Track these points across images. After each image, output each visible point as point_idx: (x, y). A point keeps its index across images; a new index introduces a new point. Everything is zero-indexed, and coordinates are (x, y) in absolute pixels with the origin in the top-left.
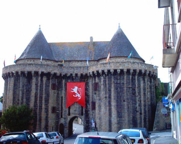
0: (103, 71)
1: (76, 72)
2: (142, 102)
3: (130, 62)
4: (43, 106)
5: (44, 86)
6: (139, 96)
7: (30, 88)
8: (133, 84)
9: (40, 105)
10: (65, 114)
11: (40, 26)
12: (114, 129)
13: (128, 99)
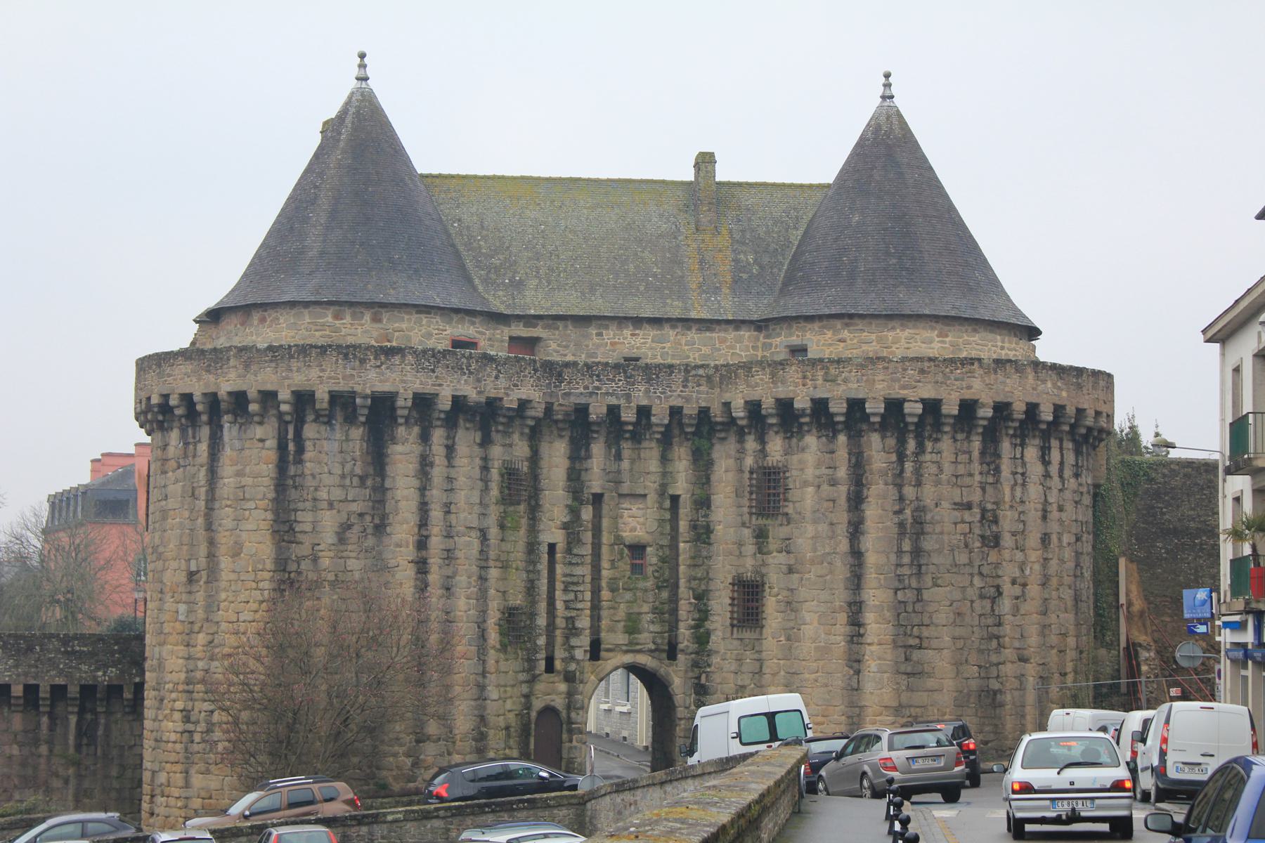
1: (640, 396)
3: (979, 360)
11: (887, 76)
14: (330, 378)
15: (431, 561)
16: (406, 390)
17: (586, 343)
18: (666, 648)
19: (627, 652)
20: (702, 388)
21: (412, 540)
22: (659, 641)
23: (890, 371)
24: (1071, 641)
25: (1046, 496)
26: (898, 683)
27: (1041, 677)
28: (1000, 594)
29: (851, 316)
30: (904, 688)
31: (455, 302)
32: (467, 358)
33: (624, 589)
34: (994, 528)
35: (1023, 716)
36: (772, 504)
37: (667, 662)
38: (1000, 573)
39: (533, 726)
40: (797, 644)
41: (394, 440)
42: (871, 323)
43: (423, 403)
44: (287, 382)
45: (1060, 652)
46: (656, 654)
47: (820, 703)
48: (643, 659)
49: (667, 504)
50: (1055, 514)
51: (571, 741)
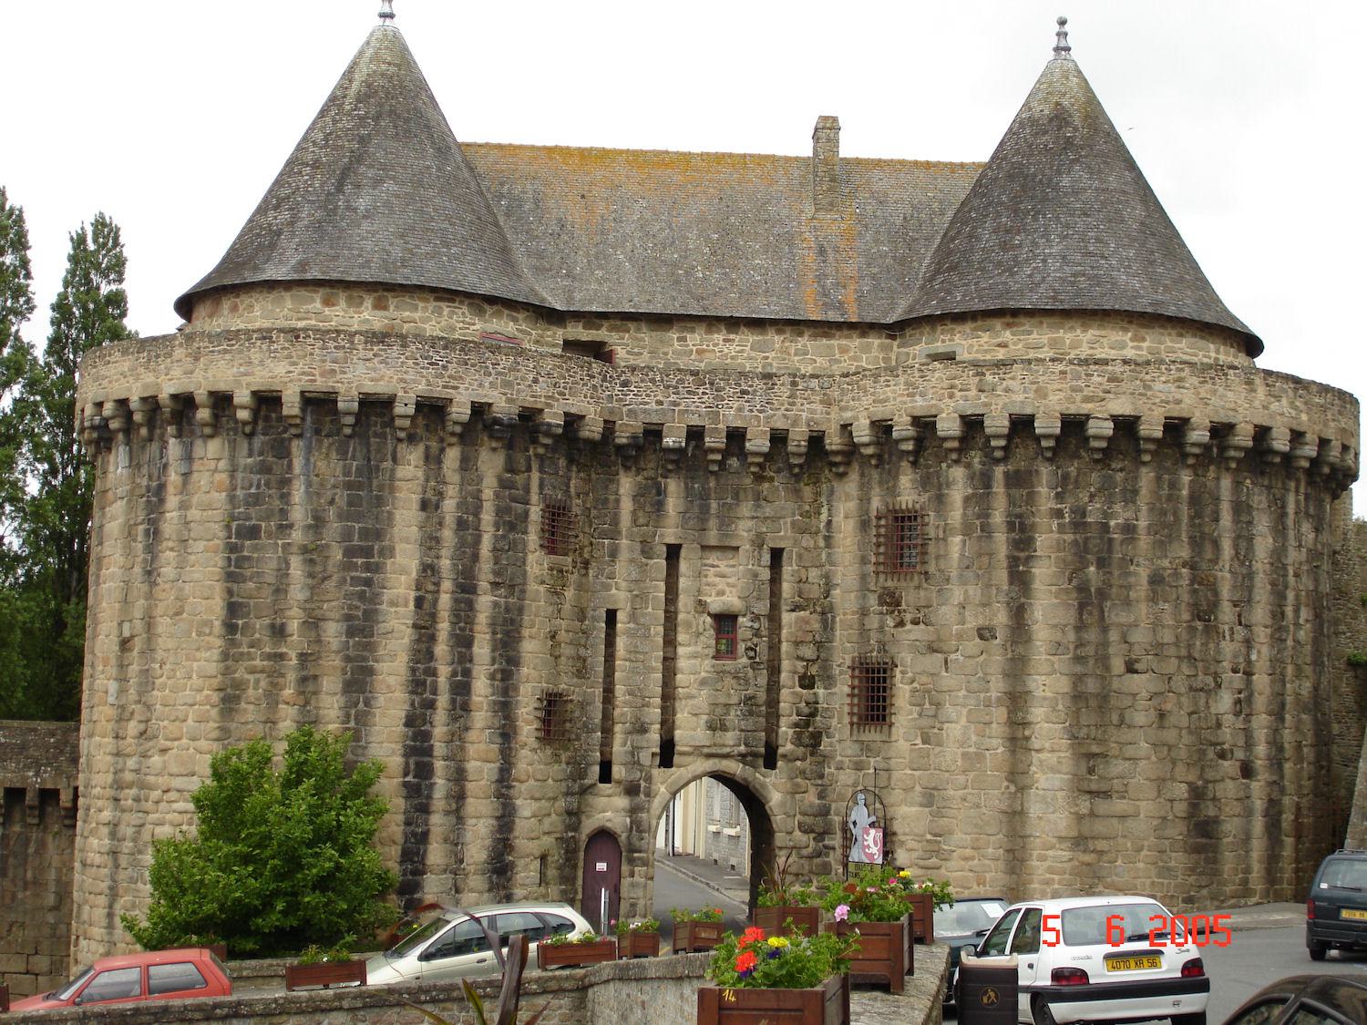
0: (972, 424)
1: (731, 415)
2: (1261, 681)
4: (482, 688)
5: (487, 517)
6: (1240, 633)
7: (378, 535)
8: (1203, 541)
9: (454, 674)
10: (635, 750)
11: (1062, 23)
13: (1158, 649)
14: (304, 373)
17: (665, 350)
18: (762, 750)
29: (1016, 313)
31: (486, 288)
36: (906, 560)
39: (582, 854)
40: (938, 749)
42: (1041, 323)
43: (433, 410)
44: (245, 380)
48: (734, 768)
49: (766, 558)
51: (632, 875)
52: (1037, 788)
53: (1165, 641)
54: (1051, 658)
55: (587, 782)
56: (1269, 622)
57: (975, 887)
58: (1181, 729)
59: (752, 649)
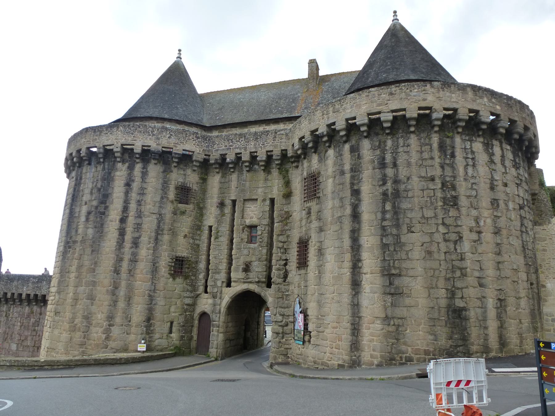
1: (251, 147)
12: (371, 341)
15: (127, 229)
16: (117, 143)
19: (244, 282)
20: (283, 140)
21: (118, 218)
22: (261, 277)
23: (370, 97)
24: (523, 276)
25: (492, 175)
26: (385, 301)
27: (499, 299)
28: (461, 238)
30: (389, 304)
32: (152, 128)
33: (243, 248)
34: (453, 193)
35: (486, 328)
37: (266, 288)
38: (459, 223)
39: (196, 322)
41: (117, 170)
45: (514, 282)
46: (260, 284)
47: (335, 314)
49: (268, 202)
50: (501, 188)
52: (365, 292)
53: (428, 216)
54: (371, 227)
55: (198, 293)
56: (490, 207)
57: (338, 342)
58: (440, 261)
59: (261, 238)
